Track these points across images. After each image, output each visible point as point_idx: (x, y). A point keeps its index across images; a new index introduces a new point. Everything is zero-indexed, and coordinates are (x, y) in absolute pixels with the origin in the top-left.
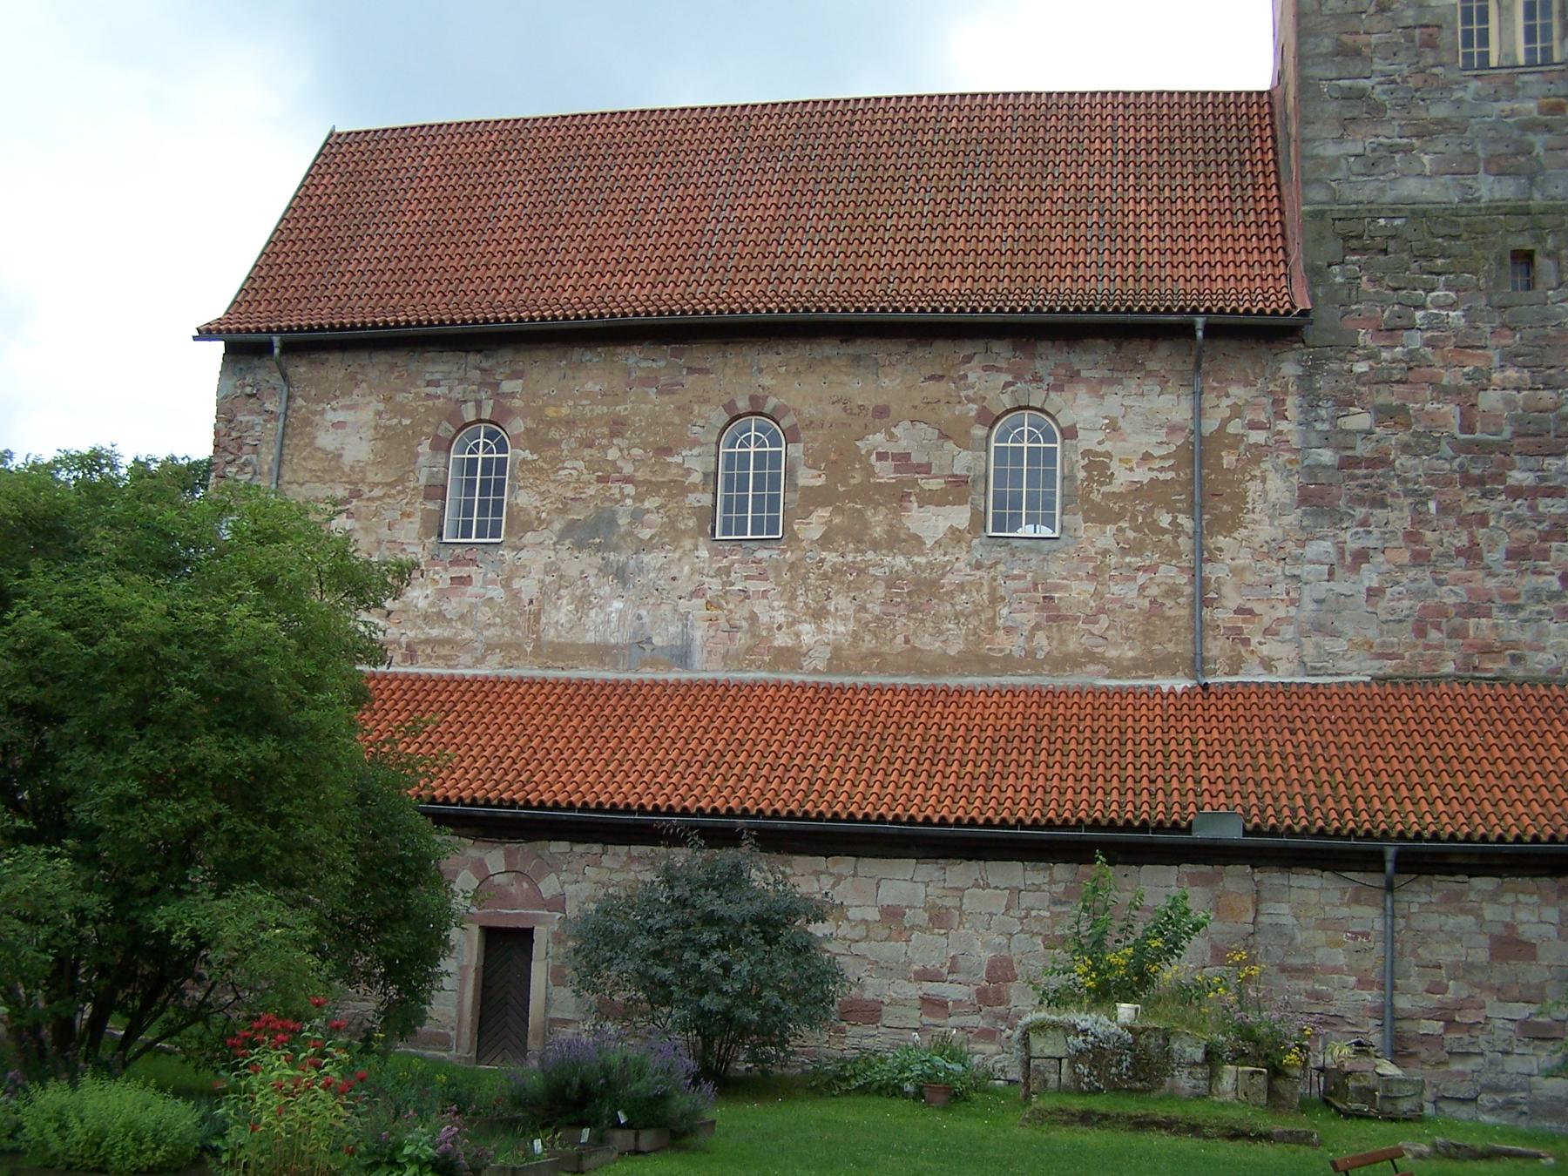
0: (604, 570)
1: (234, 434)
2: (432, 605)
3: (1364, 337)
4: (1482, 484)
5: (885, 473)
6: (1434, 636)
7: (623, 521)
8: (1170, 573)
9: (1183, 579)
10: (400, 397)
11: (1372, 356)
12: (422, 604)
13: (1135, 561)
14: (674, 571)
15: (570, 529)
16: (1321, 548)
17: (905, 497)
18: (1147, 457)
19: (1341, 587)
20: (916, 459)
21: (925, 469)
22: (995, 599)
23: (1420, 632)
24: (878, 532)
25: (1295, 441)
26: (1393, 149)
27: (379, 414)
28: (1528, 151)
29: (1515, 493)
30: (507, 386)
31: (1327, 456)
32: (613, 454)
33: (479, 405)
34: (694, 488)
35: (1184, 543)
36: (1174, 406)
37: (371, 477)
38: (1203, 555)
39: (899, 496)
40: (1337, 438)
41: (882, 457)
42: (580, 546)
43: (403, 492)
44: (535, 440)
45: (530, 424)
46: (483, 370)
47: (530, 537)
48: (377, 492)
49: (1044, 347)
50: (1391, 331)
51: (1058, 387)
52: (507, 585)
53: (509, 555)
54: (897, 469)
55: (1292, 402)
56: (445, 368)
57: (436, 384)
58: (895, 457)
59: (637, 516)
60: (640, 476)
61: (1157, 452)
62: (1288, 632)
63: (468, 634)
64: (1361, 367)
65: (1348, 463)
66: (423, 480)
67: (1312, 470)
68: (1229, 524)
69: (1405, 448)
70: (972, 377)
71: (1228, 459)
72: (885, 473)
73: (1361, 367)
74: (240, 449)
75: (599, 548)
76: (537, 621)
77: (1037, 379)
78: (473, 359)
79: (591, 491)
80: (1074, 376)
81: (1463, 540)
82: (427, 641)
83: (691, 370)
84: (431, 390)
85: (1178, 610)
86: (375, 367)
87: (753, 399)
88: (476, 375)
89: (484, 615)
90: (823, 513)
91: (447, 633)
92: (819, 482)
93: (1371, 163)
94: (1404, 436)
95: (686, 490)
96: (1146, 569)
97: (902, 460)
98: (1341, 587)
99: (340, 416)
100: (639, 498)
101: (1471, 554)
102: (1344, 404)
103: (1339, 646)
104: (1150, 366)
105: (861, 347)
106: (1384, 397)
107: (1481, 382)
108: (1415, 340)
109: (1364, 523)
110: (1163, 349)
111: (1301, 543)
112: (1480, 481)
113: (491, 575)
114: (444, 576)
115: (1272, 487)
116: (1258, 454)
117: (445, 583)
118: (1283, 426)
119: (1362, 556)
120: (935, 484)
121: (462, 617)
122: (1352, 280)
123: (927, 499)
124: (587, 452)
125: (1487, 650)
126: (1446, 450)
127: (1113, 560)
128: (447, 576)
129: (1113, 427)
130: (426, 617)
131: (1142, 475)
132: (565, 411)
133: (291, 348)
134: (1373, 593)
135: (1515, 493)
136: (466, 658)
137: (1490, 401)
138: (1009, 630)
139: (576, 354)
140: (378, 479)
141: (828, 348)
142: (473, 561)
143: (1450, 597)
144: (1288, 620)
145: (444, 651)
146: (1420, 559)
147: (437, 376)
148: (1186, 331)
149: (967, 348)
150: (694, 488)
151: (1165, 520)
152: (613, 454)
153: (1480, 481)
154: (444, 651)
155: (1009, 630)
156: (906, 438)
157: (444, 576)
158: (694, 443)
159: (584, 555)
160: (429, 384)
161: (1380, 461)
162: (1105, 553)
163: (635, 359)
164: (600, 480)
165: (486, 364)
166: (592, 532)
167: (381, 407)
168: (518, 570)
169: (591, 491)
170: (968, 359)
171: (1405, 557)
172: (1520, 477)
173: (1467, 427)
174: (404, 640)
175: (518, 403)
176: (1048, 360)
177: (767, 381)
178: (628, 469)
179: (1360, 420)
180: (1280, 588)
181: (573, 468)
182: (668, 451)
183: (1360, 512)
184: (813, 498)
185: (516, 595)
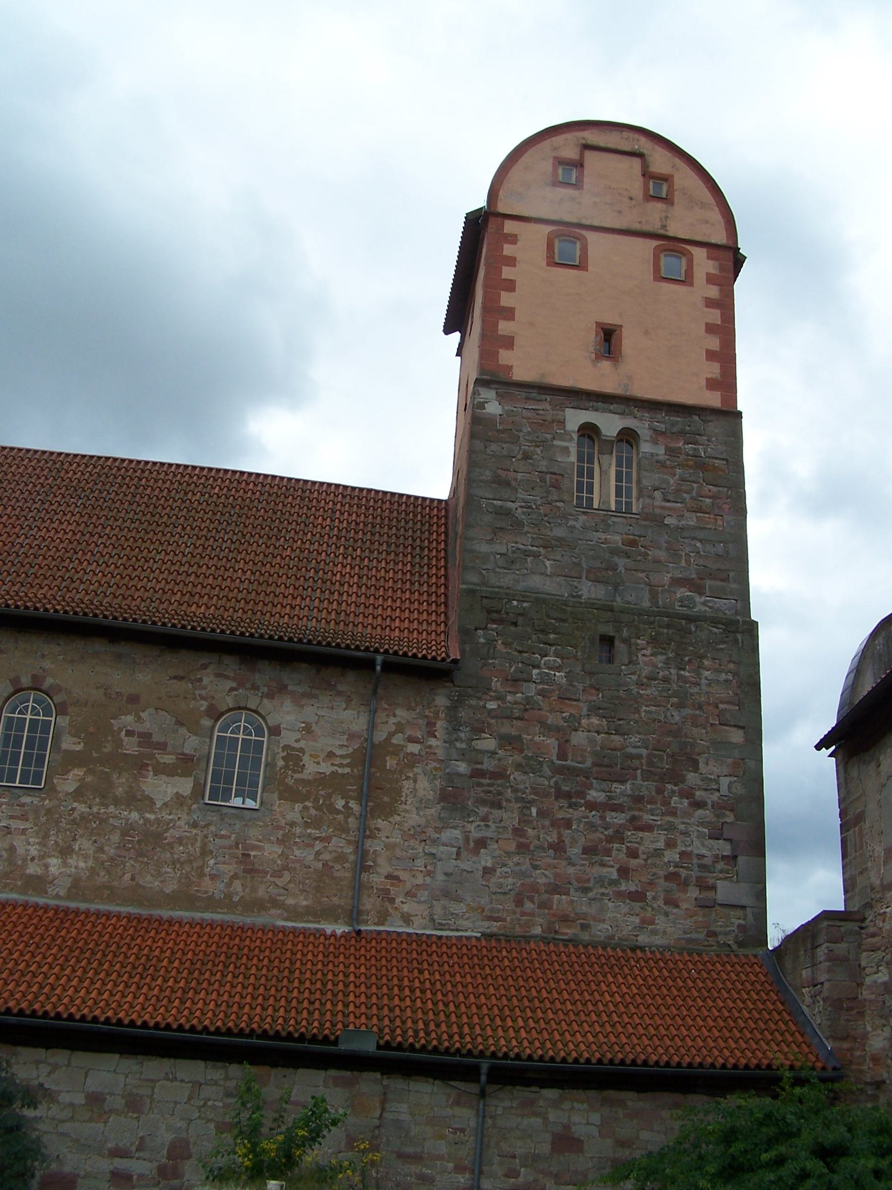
3: (496, 684)
5: (131, 747)
6: (528, 906)
9: (349, 850)
11: (500, 698)
19: (465, 865)
20: (156, 738)
21: (162, 747)
22: (205, 852)
23: (519, 902)
25: (441, 753)
26: (527, 554)
29: (592, 806)
31: (462, 767)
35: (352, 822)
36: (354, 719)
38: (366, 832)
39: (139, 766)
40: (470, 755)
41: (129, 733)
50: (515, 681)
51: (270, 696)
54: (140, 745)
55: (440, 725)
58: (140, 735)
61: (339, 752)
62: (424, 895)
64: (492, 705)
65: (478, 774)
67: (451, 777)
69: (518, 767)
70: (206, 681)
71: (391, 763)
72: (131, 747)
73: (492, 705)
77: (255, 688)
81: (553, 838)
85: (343, 873)
87: (34, 677)
90: (79, 772)
92: (78, 748)
93: (511, 561)
94: (518, 758)
96: (322, 839)
97: (145, 738)
101: (559, 848)
102: (478, 730)
104: (341, 687)
105: (122, 648)
106: (507, 728)
107: (574, 725)
108: (531, 690)
109: (485, 819)
110: (351, 676)
111: (438, 830)
112: (568, 795)
115: (421, 786)
116: (413, 760)
118: (433, 742)
119: (482, 843)
122: (491, 642)
123: (168, 771)
125: (565, 919)
126: (546, 770)
127: (298, 830)
131: (326, 768)
135: (592, 806)
137: (579, 738)
138: (213, 877)
141: (99, 646)
143: (541, 878)
144: (424, 886)
146: (523, 848)
151: (340, 804)
156: (150, 721)
162: (292, 824)
170: (205, 667)
171: (512, 847)
172: (594, 795)
173: (562, 756)
179: (488, 743)
180: (420, 862)
184: (71, 760)
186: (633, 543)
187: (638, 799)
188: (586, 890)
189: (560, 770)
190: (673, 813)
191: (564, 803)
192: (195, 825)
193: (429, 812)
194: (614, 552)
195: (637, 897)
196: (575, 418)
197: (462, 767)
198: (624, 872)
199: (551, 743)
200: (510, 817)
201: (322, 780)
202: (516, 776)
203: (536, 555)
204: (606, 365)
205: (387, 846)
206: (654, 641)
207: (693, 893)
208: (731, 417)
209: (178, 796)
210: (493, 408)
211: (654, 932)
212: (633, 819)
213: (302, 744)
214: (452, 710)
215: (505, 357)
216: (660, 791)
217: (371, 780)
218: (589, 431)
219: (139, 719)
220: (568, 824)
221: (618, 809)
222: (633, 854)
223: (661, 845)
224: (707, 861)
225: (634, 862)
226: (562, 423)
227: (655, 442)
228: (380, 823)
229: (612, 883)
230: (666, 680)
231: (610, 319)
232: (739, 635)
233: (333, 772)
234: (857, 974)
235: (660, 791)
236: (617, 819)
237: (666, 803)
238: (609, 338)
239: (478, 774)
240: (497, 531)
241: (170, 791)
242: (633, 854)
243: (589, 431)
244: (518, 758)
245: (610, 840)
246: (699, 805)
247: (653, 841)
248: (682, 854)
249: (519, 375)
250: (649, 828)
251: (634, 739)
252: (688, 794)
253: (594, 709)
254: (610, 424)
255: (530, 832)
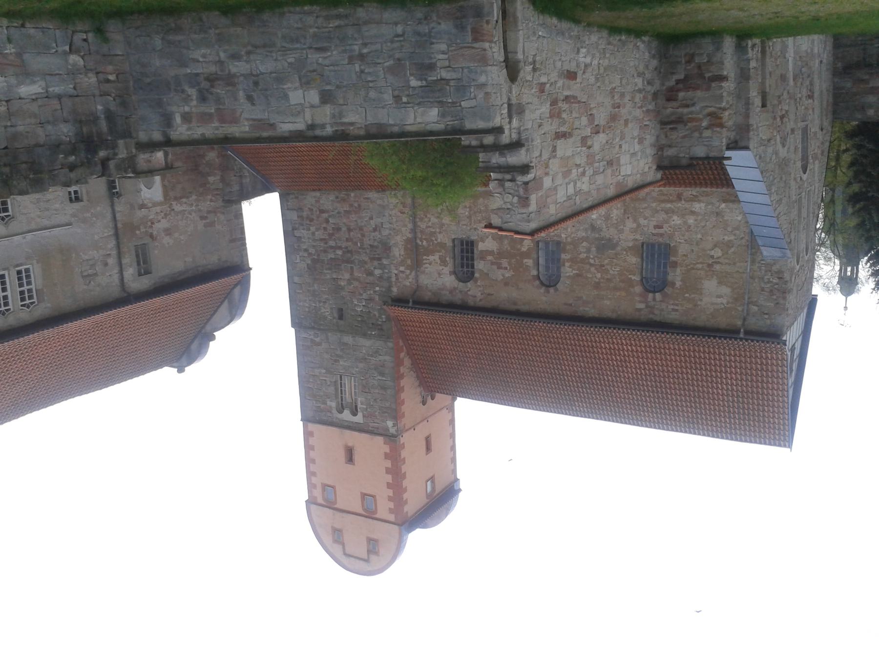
0: (600, 230)
1: (775, 297)
2: (671, 217)
3: (377, 298)
4: (348, 251)
5: (505, 263)
6: (356, 205)
7: (594, 249)
8: (423, 225)
9: (419, 223)
10: (690, 306)
11: (375, 292)
12: (675, 218)
13: (432, 230)
14: (574, 229)
15: (614, 246)
16: (385, 233)
17: (499, 254)
18: (430, 264)
19: (379, 220)
20: (495, 267)
21: (492, 263)
22: (469, 217)
23: (359, 206)
24: (506, 242)
25: (392, 267)
26: (372, 356)
27: (701, 300)
28: (342, 350)
29: (340, 248)
30: (642, 306)
31: (385, 262)
32: (599, 275)
33: (654, 299)
34: (568, 261)
35: (419, 235)
36: (424, 280)
37: (703, 272)
38: (414, 231)
39: (501, 254)
40: (382, 267)
41: (506, 268)
42: (610, 240)
43: (687, 266)
44: (631, 283)
45: (632, 290)
46: (653, 314)
47: (631, 244)
48: (700, 266)
49: (459, 302)
50: (371, 299)
51: (455, 289)
52: (639, 225)
53: (638, 237)
54: (501, 264)
55: (393, 279)
56: (671, 317)
57: (673, 310)
58: (501, 268)
59: (588, 251)
60: (588, 267)
61: (427, 265)
62: (391, 206)
63: (654, 205)
64: (377, 289)
65: (379, 259)
66: (678, 270)
67: (388, 257)
68: (408, 241)
69: (366, 263)
70: (479, 294)
71: (409, 262)
72: (505, 263)
73: (377, 289)
74: (771, 291)
75: (602, 239)
76: (625, 211)
77: (461, 292)
78: (658, 319)
79: (606, 261)
80: (451, 292)
81: (352, 233)
82: (671, 202)
83: (571, 305)
84: (676, 308)
85: (420, 213)
86: (702, 320)
87: (548, 292)
88: (657, 312)
89: (647, 213)
90: (524, 249)
91: (663, 205)
92: (525, 260)
93: (377, 352)
94: (367, 266)
95: (572, 260)
96: (429, 227)
97: (499, 268)
98: (379, 220)
99: (719, 300)
100: (588, 258)
101: (349, 230)
102: (381, 277)
103: (379, 202)
104: (430, 294)
105: (513, 308)
106: (371, 278)
107: (349, 282)
108: (365, 296)
109: (375, 240)
110: (427, 298)
111: (390, 234)
112: (348, 252)
113: (646, 229)
114: (666, 229)
115: (398, 252)
116: (402, 263)
117: (665, 226)
118: (396, 272)
119: (375, 230)
120: (490, 258)
121: (657, 212)
122: (380, 317)
123: (491, 253)
124: (609, 277)
125: (344, 200)
126: (356, 261)
127: (438, 230)
128: (665, 229)
129: (439, 274)
130: (673, 212)
131: (431, 258)
132: (618, 294)
133: (737, 332)
134: (371, 218)
135: (340, 248)
136: (654, 194)
137: (347, 276)
138: (466, 207)
139: (614, 316)
140: (699, 272)
141: (524, 308)
142: (654, 235)
143: (353, 217)
144: (392, 210)
145: (663, 198)
146: (361, 229)
147: (673, 313)
148: (415, 302)
149: (480, 304)
150: (568, 261)
151: (425, 243)
152: (599, 275)
153: (348, 252)
154: (663, 198)
155: (466, 207)
156: (499, 275)
157: (666, 229)
158: (569, 277)
159: (608, 236)
160: (677, 310)
161: (372, 259)
162: (440, 233)
163: (591, 311)
164: (603, 266)
165: (651, 316)
166: (605, 245)
167: (699, 303)
168: (634, 231)
169: (606, 261)
170: (481, 300)
171: (365, 229)
172: (339, 252)
173: (352, 268)
174: (683, 202)
175: (637, 298)
176: (457, 298)
177: (544, 298)
178: (593, 269)
179: (377, 272)
180: (394, 220)
181: (614, 271)
182: (578, 275)
183: (376, 244)
184: (527, 255)
185: (635, 220)
186: (336, 361)
187: (325, 251)
188: (339, 213)
189: (352, 262)
190: (314, 246)
191: (350, 249)
192: (475, 229)
193: (393, 242)
194: (341, 357)
195: (322, 211)
196: (359, 418)
197: (385, 262)
198: (327, 221)
199: (356, 274)
200: (367, 242)
201: (431, 252)
202: (366, 259)
203: (368, 355)
204: (350, 444)
205: (406, 226)
206: (325, 318)
207: (305, 214)
208: (305, 419)
209: (483, 241)
210: (390, 424)
211: (315, 197)
212: (326, 243)
213: (441, 268)
214: (389, 288)
215: (386, 449)
216: (318, 255)
217: (416, 253)
218: (354, 413)
219: (503, 275)
220: (347, 240)
221: (332, 247)
222: (325, 229)
223: (317, 233)
224: (301, 227)
225: (324, 225)
226: (364, 416)
227: (331, 407)
228: (410, 236)
229: (330, 216)
230: (320, 302)
231: (350, 466)
232: (303, 320)
233: (528, 173)
234: (223, 180)
235: (318, 255)
236: (332, 243)
237: (316, 251)
238: (350, 455)
239: (379, 259)
240: (383, 366)
241: (486, 243)
242: (325, 229)
243: (354, 413)
244: (367, 266)
245: (333, 234)
246: (306, 250)
247: (319, 234)
248: (309, 230)
249: (380, 440)
250: (321, 240)
251: (328, 277)
252: (310, 254)
253: (342, 288)
254: (347, 415)
255: (359, 236)
